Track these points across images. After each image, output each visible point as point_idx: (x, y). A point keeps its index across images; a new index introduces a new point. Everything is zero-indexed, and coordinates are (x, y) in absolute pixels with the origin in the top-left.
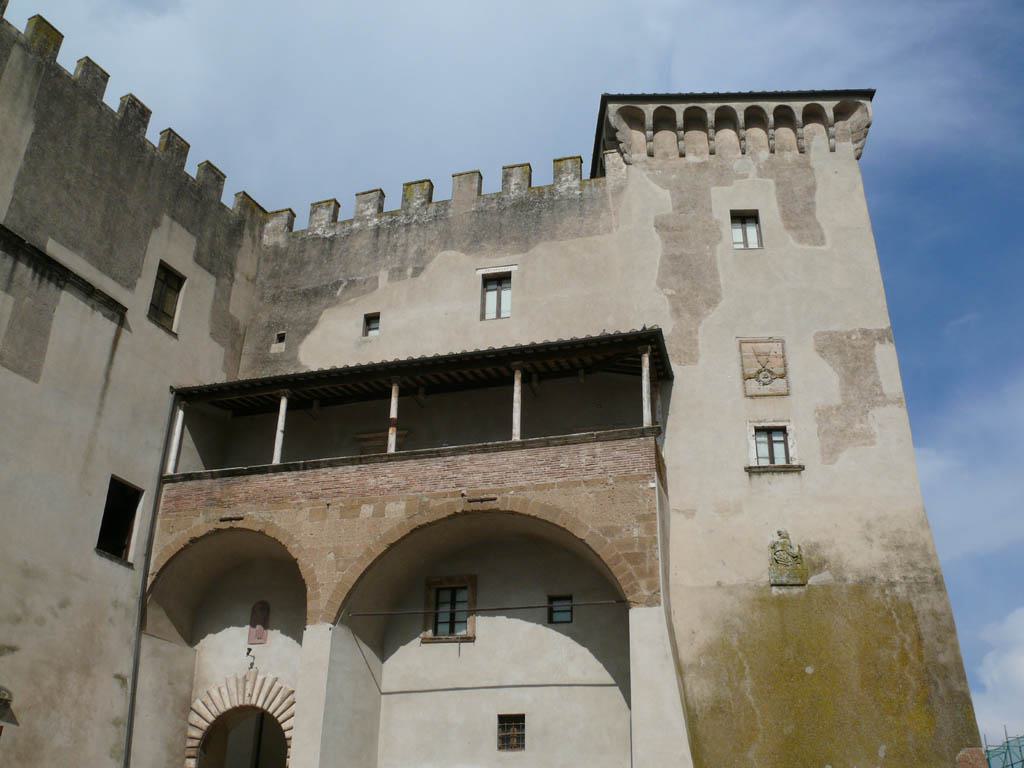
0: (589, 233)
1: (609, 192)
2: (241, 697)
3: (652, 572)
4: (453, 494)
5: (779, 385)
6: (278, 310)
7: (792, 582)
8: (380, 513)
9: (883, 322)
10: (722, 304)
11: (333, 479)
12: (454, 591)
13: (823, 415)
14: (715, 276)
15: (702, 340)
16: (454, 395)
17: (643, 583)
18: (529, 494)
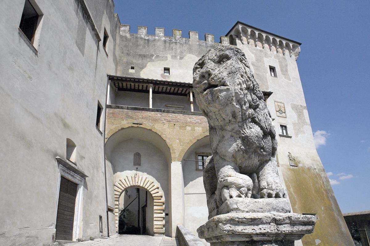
2: (134, 183)
6: (130, 58)
7: (295, 165)
11: (175, 117)
12: (203, 156)
13: (294, 124)
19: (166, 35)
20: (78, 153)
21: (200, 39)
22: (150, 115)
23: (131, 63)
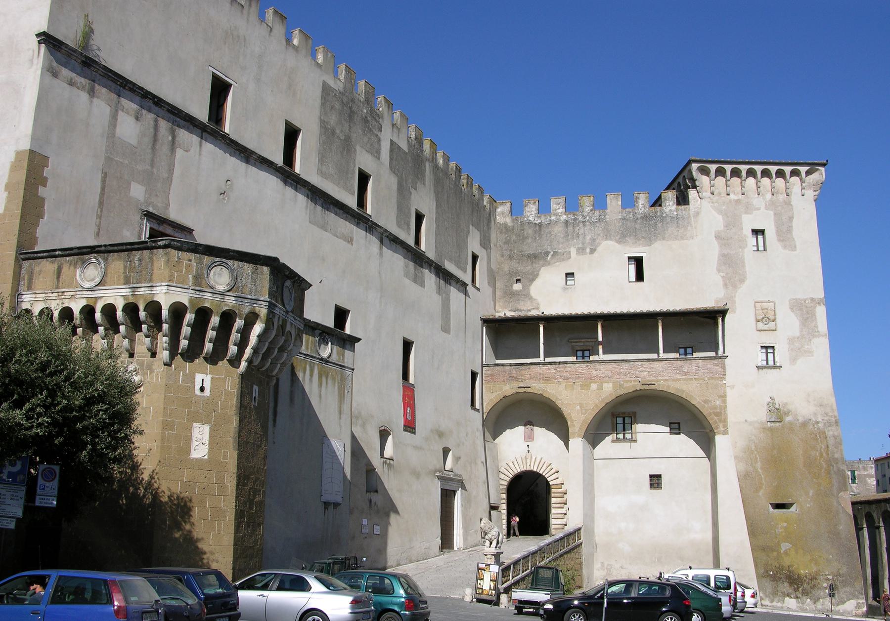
0: (682, 238)
1: (692, 213)
3: (725, 421)
4: (635, 381)
5: (772, 325)
6: (514, 264)
8: (600, 388)
9: (821, 294)
10: (747, 282)
13: (791, 340)
14: (744, 266)
15: (737, 299)
16: (630, 330)
17: (721, 425)
18: (670, 383)
19: (567, 210)
20: (454, 456)
21: (624, 207)
22: (540, 371)
23: (517, 273)
